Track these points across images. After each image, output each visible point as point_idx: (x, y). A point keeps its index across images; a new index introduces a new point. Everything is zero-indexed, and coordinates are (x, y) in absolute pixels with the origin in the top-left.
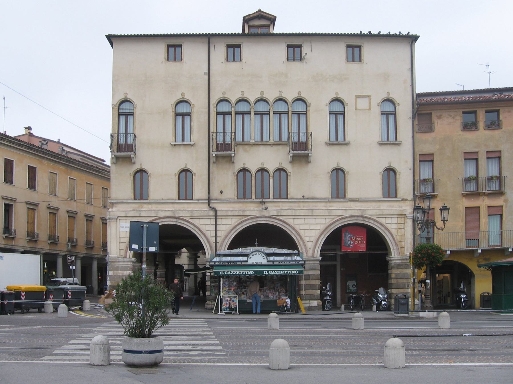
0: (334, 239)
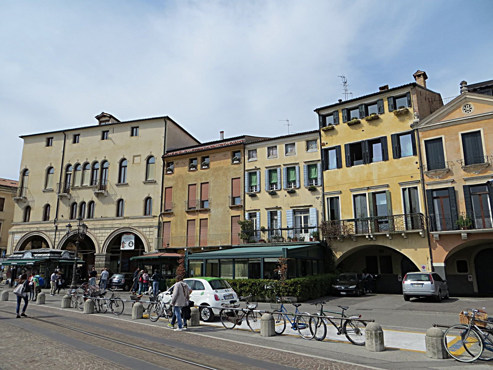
0: (116, 241)
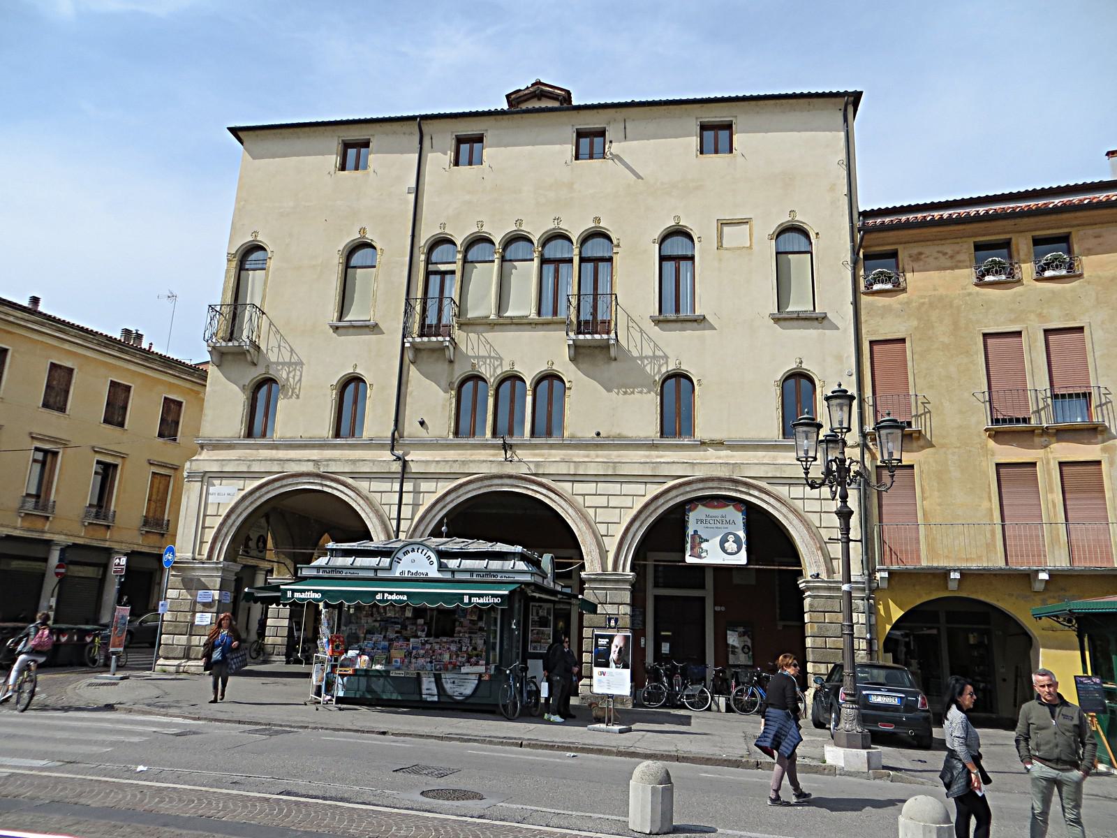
0: (665, 532)
